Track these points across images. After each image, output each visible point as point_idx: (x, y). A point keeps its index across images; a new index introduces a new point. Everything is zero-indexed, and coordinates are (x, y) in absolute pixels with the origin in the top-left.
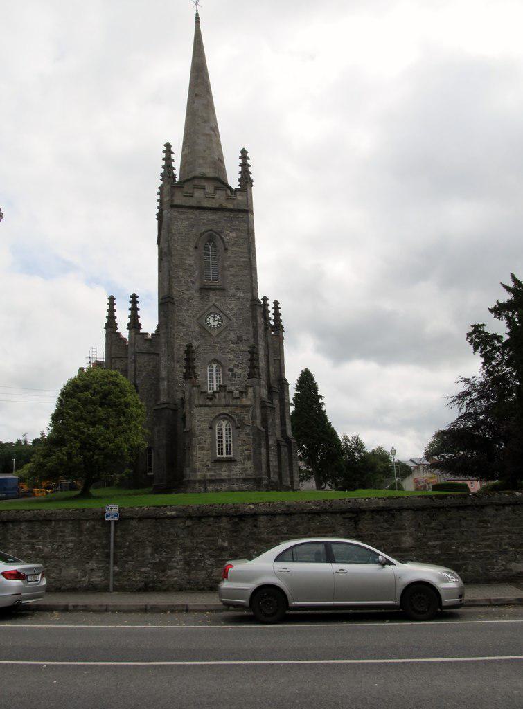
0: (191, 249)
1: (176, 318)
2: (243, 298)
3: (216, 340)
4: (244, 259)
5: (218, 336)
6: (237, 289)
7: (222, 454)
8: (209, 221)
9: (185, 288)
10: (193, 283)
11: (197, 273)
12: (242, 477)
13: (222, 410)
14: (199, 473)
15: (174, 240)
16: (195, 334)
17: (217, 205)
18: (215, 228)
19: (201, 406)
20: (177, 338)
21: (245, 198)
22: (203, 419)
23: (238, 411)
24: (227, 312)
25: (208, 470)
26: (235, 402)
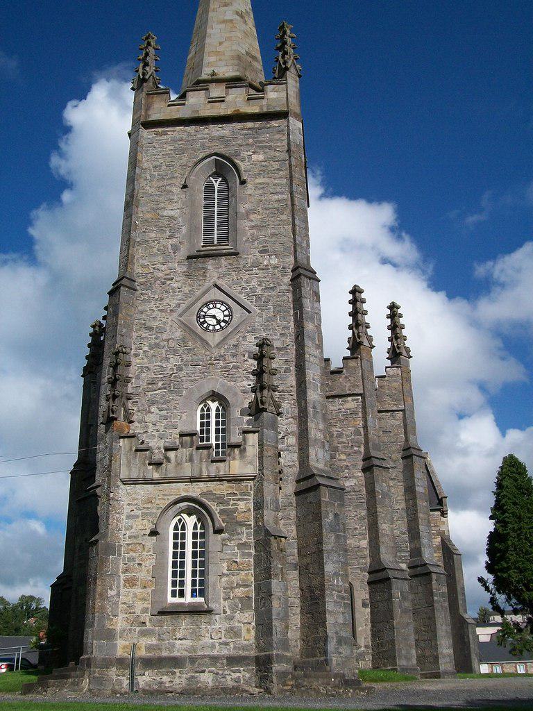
0: (176, 189)
1: (138, 316)
2: (275, 268)
3: (216, 352)
4: (280, 197)
5: (219, 345)
6: (264, 251)
7: (182, 594)
8: (211, 140)
9: (160, 259)
10: (176, 249)
11: (184, 230)
12: (225, 652)
13: (183, 490)
14: (120, 643)
15: (146, 179)
16: (173, 344)
17: (229, 112)
18: (222, 150)
19: (135, 482)
20: (136, 355)
21: (283, 95)
22: (139, 513)
23: (222, 489)
24: (242, 296)
25: (144, 634)
26: (213, 469)
